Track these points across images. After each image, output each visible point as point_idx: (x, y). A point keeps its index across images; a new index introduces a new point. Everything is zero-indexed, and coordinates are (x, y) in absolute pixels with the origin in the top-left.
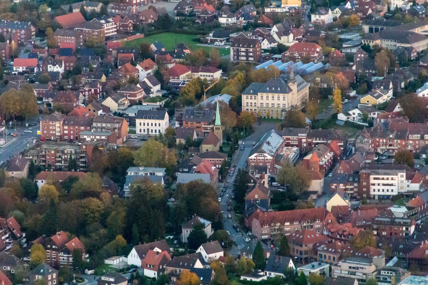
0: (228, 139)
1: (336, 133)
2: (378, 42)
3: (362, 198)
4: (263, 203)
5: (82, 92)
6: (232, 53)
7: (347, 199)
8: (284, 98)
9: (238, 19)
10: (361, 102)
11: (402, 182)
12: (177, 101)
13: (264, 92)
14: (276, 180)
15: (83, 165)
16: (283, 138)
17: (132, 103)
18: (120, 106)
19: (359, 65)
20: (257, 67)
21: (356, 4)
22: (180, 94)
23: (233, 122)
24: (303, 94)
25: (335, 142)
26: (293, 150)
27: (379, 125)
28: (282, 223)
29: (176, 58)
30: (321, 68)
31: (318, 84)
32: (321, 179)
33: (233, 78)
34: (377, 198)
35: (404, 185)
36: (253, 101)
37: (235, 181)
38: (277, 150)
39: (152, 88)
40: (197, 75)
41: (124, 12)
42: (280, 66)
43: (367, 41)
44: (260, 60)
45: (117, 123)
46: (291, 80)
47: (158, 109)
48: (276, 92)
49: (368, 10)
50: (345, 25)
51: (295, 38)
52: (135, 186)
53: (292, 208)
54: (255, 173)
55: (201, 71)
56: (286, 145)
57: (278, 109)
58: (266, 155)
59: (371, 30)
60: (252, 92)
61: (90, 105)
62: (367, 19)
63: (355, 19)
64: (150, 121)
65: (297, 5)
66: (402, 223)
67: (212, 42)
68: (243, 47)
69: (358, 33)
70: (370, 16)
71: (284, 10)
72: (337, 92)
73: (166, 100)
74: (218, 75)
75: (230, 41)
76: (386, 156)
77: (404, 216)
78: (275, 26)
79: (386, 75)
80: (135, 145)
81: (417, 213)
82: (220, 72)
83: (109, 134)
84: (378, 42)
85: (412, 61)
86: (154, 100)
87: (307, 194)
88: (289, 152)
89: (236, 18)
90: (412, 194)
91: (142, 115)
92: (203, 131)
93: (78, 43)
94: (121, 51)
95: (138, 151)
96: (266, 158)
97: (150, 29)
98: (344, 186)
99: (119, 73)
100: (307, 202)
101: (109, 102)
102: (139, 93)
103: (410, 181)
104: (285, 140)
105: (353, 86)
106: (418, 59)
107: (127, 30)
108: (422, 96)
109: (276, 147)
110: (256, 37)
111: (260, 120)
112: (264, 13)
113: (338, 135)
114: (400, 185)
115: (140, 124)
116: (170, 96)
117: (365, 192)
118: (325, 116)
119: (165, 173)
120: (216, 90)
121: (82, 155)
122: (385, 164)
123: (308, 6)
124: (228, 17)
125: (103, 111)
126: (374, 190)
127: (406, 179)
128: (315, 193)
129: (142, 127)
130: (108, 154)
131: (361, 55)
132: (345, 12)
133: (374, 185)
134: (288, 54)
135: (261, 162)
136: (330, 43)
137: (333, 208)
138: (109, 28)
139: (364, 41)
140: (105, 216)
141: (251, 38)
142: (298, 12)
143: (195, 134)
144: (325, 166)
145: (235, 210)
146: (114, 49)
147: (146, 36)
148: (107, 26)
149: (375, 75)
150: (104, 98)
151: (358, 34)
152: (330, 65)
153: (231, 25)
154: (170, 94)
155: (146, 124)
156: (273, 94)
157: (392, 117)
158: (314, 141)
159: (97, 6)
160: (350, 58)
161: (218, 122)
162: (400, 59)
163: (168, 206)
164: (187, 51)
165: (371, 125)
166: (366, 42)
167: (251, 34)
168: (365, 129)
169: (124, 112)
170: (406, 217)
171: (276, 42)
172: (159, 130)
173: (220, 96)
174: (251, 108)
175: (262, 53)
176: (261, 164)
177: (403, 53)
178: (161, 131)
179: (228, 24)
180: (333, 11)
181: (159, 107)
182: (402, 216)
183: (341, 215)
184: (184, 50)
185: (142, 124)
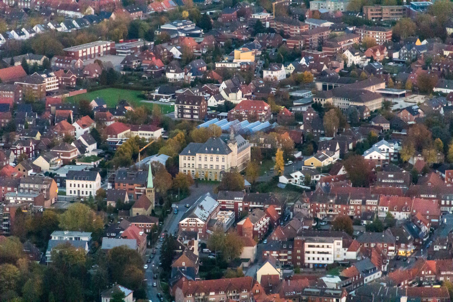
0: (161, 202)
1: (274, 198)
2: (330, 100)
3: (296, 266)
4: (190, 271)
5: (13, 150)
6: (176, 110)
7: (278, 268)
8: (223, 159)
9: (186, 74)
10: (305, 164)
11: (338, 250)
12: (112, 161)
13: (186, 155)
14: (207, 246)
15: (6, 228)
16: (219, 202)
17: (66, 163)
18: (52, 165)
19: (307, 125)
20: (200, 125)
21: (311, 60)
22: (116, 154)
23: (167, 184)
24: (244, 155)
25: (271, 206)
26: (228, 214)
27: (319, 188)
28: (207, 293)
29: (117, 115)
30: (268, 127)
31: (261, 145)
32: (253, 246)
33: (172, 137)
34: (311, 266)
35: (340, 253)
36: (191, 162)
37: (163, 247)
38: (210, 215)
39: (87, 147)
40: (136, 134)
41: (68, 66)
42: (224, 125)
43: (319, 100)
44: (206, 117)
45: (45, 184)
46: (231, 140)
47: (91, 170)
48: (215, 152)
49: (322, 66)
50: (297, 82)
51: (244, 95)
52: (58, 251)
53: (219, 276)
54: (183, 239)
55: (141, 130)
56: (221, 210)
57: (217, 171)
58: (197, 219)
59: (324, 87)
60: (189, 152)
61: (20, 164)
62: (321, 76)
63: (308, 76)
64: (81, 182)
65: (250, 61)
66: (332, 294)
67: (158, 98)
68: (188, 104)
69: (309, 90)
70: (325, 73)
71: (236, 66)
72: (280, 152)
73: (101, 160)
74: (158, 133)
75: (176, 98)
76: (325, 222)
77: (337, 287)
78: (223, 82)
79: (336, 135)
80: (62, 208)
81: (351, 284)
82: (162, 130)
83: (36, 196)
84: (330, 100)
85: (364, 121)
86: (88, 160)
87: (239, 261)
88: (223, 217)
89: (184, 73)
90: (348, 263)
91: (72, 175)
92: (136, 193)
93: (16, 98)
94: (61, 107)
95: (63, 215)
96: (198, 223)
97: (92, 84)
98: (277, 253)
99: (54, 131)
100: (236, 271)
101: (41, 162)
102: (73, 152)
103: (347, 249)
104: (220, 204)
105: (298, 147)
106: (370, 119)
107: (69, 85)
108: (369, 158)
109: (210, 211)
110: (203, 94)
111: (197, 181)
112: (214, 68)
113: (276, 199)
114: (336, 253)
115: (71, 185)
116: (106, 156)
117: (299, 261)
118: (266, 178)
119: (90, 238)
120: (153, 149)
121: (5, 218)
122: (322, 230)
123: (261, 62)
124: (176, 72)
125: (34, 171)
126: (309, 259)
127: (343, 247)
128: (247, 260)
129: (73, 189)
130: (32, 217)
131: (310, 114)
132: (299, 68)
133: (308, 252)
134: (234, 112)
135: (192, 227)
136: (280, 101)
137: (263, 277)
138: (51, 82)
139: (316, 99)
140: (21, 283)
141: (197, 94)
142: (250, 68)
143: (127, 196)
144: (260, 232)
145: (161, 278)
146: (52, 105)
147: (90, 91)
148: (48, 81)
149: (323, 135)
150: (36, 156)
151: (310, 92)
152: (278, 124)
153: (179, 80)
154: (106, 153)
155: (77, 186)
156: (211, 155)
157: (335, 181)
158: (250, 206)
159: (40, 59)
160: (299, 117)
161: (150, 184)
162: (351, 119)
163: (89, 274)
164: (129, 108)
165: (313, 188)
166: (317, 100)
167: (198, 91)
168: (304, 193)
169: (55, 172)
170: (339, 288)
171: (224, 99)
172: (91, 192)
173: (157, 156)
174: (188, 169)
175: (208, 110)
176: (192, 230)
177: (356, 112)
178: (92, 194)
179: (176, 80)
180: (287, 67)
181: (93, 167)
182: (335, 286)
183: (270, 285)
184: (125, 107)
185: (73, 185)
